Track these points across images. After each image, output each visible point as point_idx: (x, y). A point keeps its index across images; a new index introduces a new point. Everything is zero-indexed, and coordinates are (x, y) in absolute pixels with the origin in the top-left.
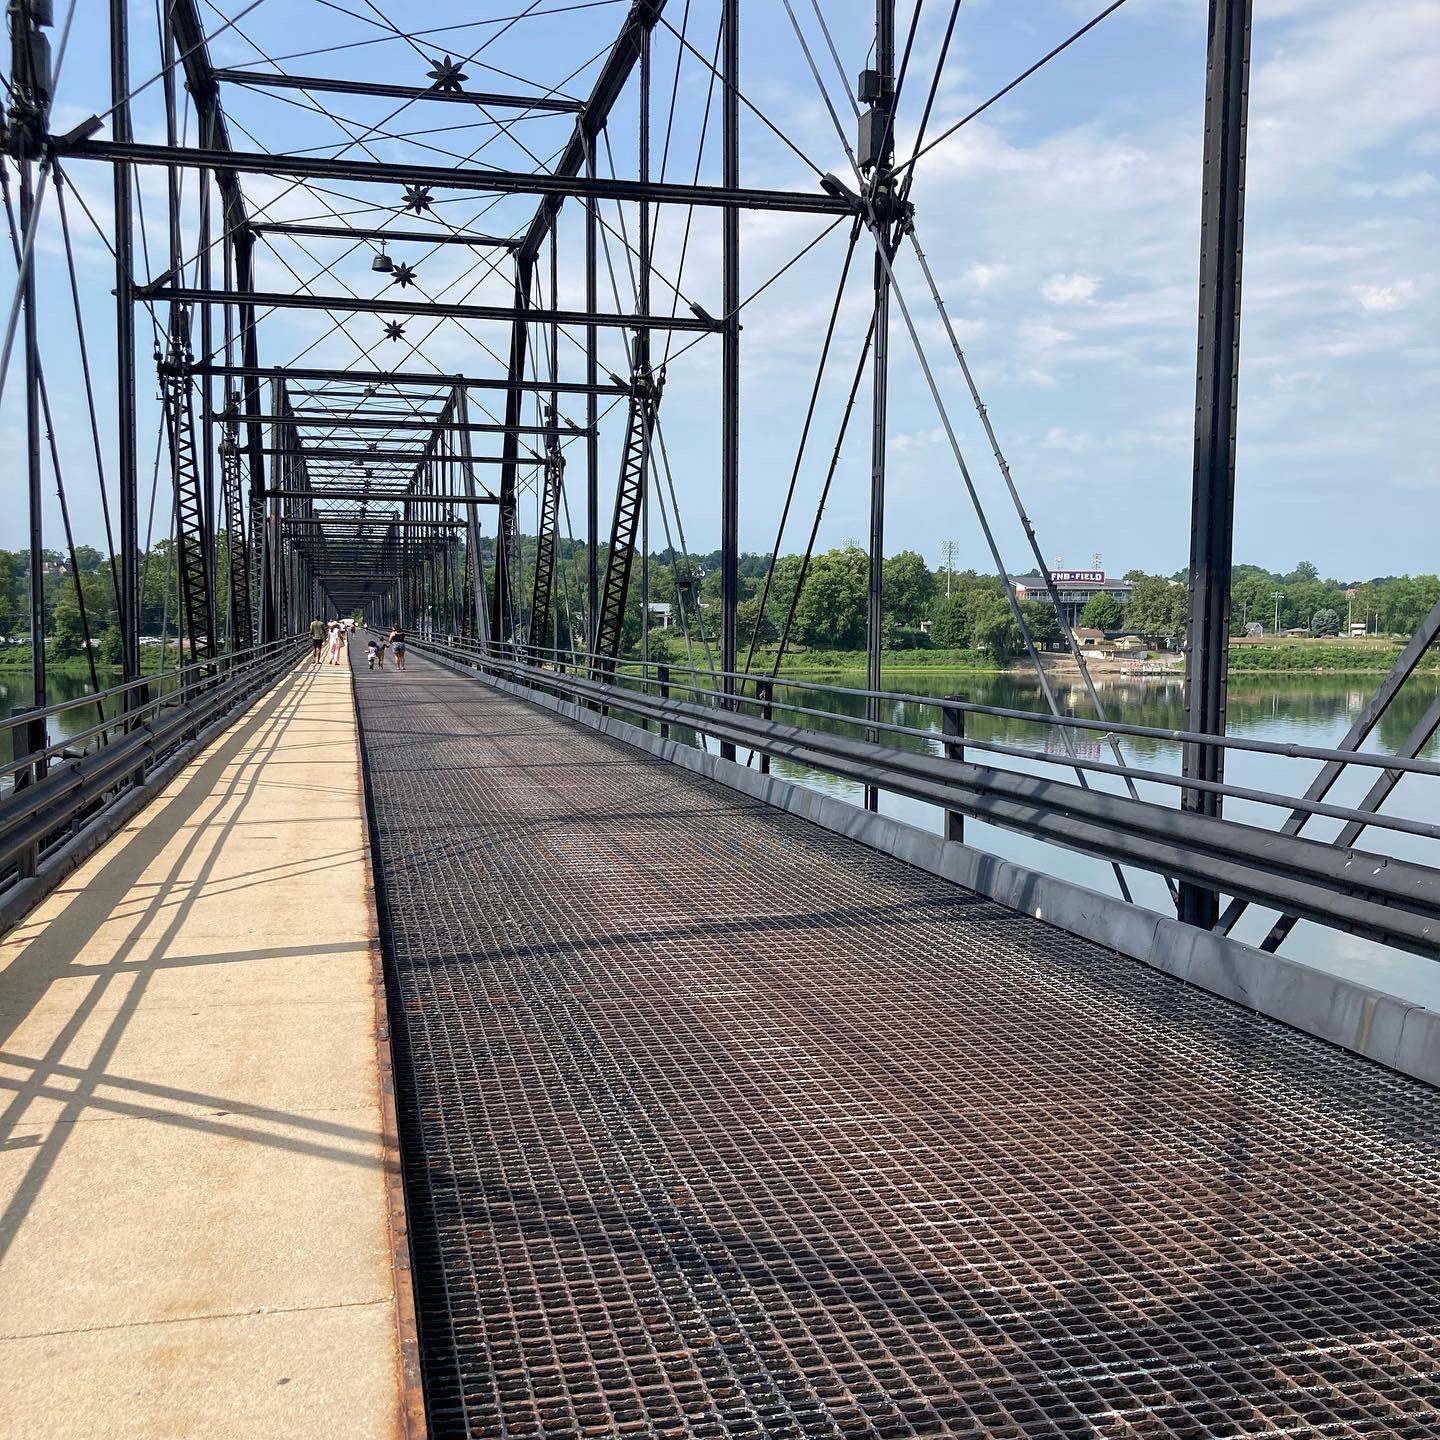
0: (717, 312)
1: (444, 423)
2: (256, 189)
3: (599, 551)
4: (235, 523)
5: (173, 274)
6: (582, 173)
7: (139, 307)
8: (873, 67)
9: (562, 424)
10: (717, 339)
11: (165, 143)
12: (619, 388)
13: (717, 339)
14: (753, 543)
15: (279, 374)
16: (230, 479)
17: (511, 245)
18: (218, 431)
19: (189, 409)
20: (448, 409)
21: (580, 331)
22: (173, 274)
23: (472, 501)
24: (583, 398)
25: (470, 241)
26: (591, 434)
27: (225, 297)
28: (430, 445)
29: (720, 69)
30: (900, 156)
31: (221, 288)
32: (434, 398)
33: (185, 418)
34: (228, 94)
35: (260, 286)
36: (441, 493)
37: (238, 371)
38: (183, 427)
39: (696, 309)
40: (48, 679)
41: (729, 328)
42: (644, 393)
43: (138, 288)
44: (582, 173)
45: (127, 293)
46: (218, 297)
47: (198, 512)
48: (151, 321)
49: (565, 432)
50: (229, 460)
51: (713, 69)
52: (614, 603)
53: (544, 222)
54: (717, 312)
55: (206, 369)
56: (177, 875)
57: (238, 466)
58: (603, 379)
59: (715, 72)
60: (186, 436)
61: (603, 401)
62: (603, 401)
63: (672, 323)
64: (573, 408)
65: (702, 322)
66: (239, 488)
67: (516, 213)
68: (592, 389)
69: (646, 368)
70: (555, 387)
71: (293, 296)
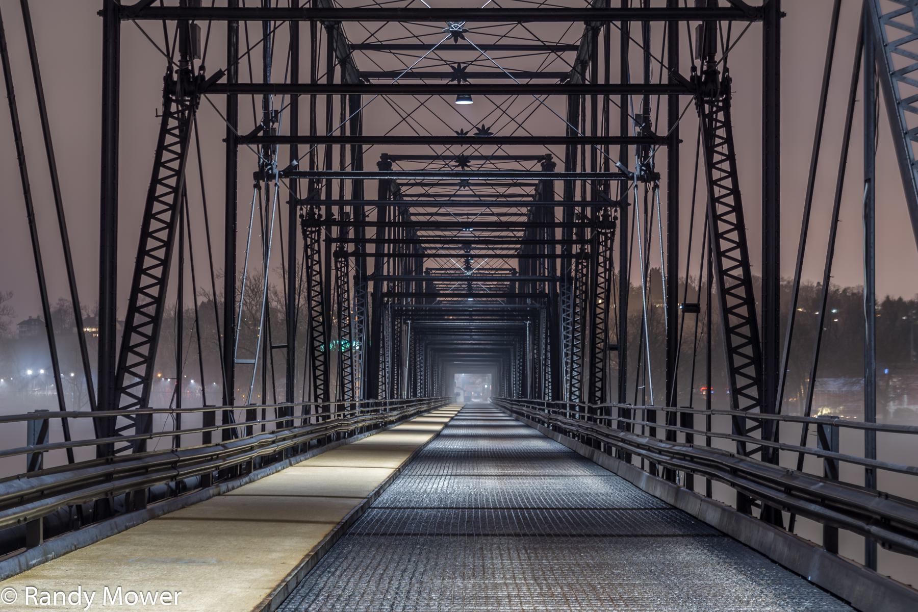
2: (353, 31)
4: (308, 233)
7: (242, 149)
11: (250, 82)
16: (341, 276)
18: (334, 247)
19: (319, 252)
27: (342, 140)
29: (543, 6)
31: (586, 146)
33: (316, 257)
35: (367, 131)
36: (392, 207)
37: (348, 203)
38: (315, 263)
43: (334, 239)
46: (336, 140)
47: (321, 293)
50: (341, 262)
51: (543, 4)
52: (601, 321)
57: (347, 265)
59: (541, 4)
60: (316, 268)
66: (347, 274)
71: (384, 137)
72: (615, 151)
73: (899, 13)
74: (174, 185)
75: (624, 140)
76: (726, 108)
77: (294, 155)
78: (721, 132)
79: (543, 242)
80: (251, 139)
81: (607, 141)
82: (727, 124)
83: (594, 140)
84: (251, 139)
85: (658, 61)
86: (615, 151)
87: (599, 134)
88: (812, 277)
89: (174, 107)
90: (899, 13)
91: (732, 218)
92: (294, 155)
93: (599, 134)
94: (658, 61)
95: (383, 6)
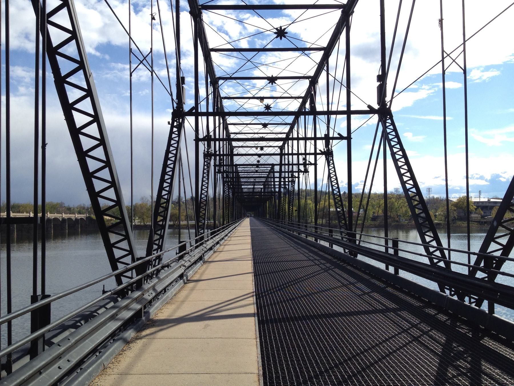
0: (345, 134)
1: (270, 172)
3: (318, 192)
5: (196, 107)
6: (291, 136)
7: (200, 143)
8: (327, 133)
9: (307, 162)
10: (345, 142)
12: (322, 153)
13: (345, 142)
14: (357, 189)
15: (236, 165)
17: (279, 147)
20: (271, 169)
21: (296, 156)
22: (196, 107)
23: (315, 154)
24: (313, 156)
25: (292, 98)
26: (315, 164)
28: (268, 175)
30: (388, 99)
32: (269, 167)
34: (214, 55)
39: (339, 134)
40: (334, 205)
41: (349, 138)
42: (328, 154)
44: (291, 136)
45: (197, 140)
48: (202, 146)
49: (308, 164)
53: (284, 144)
54: (345, 134)
55: (215, 155)
56: (303, 101)
58: (318, 151)
61: (318, 156)
62: (318, 156)
63: (334, 138)
64: (311, 159)
65: (341, 137)
67: (290, 119)
68: (315, 154)
69: (329, 148)
70: (306, 154)
72: (295, 157)
73: (438, 262)
74: (175, 153)
75: (215, 140)
76: (333, 158)
77: (209, 146)
78: (331, 162)
79: (271, 178)
80: (203, 139)
81: (293, 154)
82: (333, 160)
83: (288, 154)
84: (203, 139)
85: (132, 53)
86: (295, 157)
87: (221, 138)
88: (304, 188)
89: (175, 124)
90: (438, 262)
91: (333, 169)
92: (209, 146)
93: (221, 138)
94: (132, 53)
95: (231, 96)
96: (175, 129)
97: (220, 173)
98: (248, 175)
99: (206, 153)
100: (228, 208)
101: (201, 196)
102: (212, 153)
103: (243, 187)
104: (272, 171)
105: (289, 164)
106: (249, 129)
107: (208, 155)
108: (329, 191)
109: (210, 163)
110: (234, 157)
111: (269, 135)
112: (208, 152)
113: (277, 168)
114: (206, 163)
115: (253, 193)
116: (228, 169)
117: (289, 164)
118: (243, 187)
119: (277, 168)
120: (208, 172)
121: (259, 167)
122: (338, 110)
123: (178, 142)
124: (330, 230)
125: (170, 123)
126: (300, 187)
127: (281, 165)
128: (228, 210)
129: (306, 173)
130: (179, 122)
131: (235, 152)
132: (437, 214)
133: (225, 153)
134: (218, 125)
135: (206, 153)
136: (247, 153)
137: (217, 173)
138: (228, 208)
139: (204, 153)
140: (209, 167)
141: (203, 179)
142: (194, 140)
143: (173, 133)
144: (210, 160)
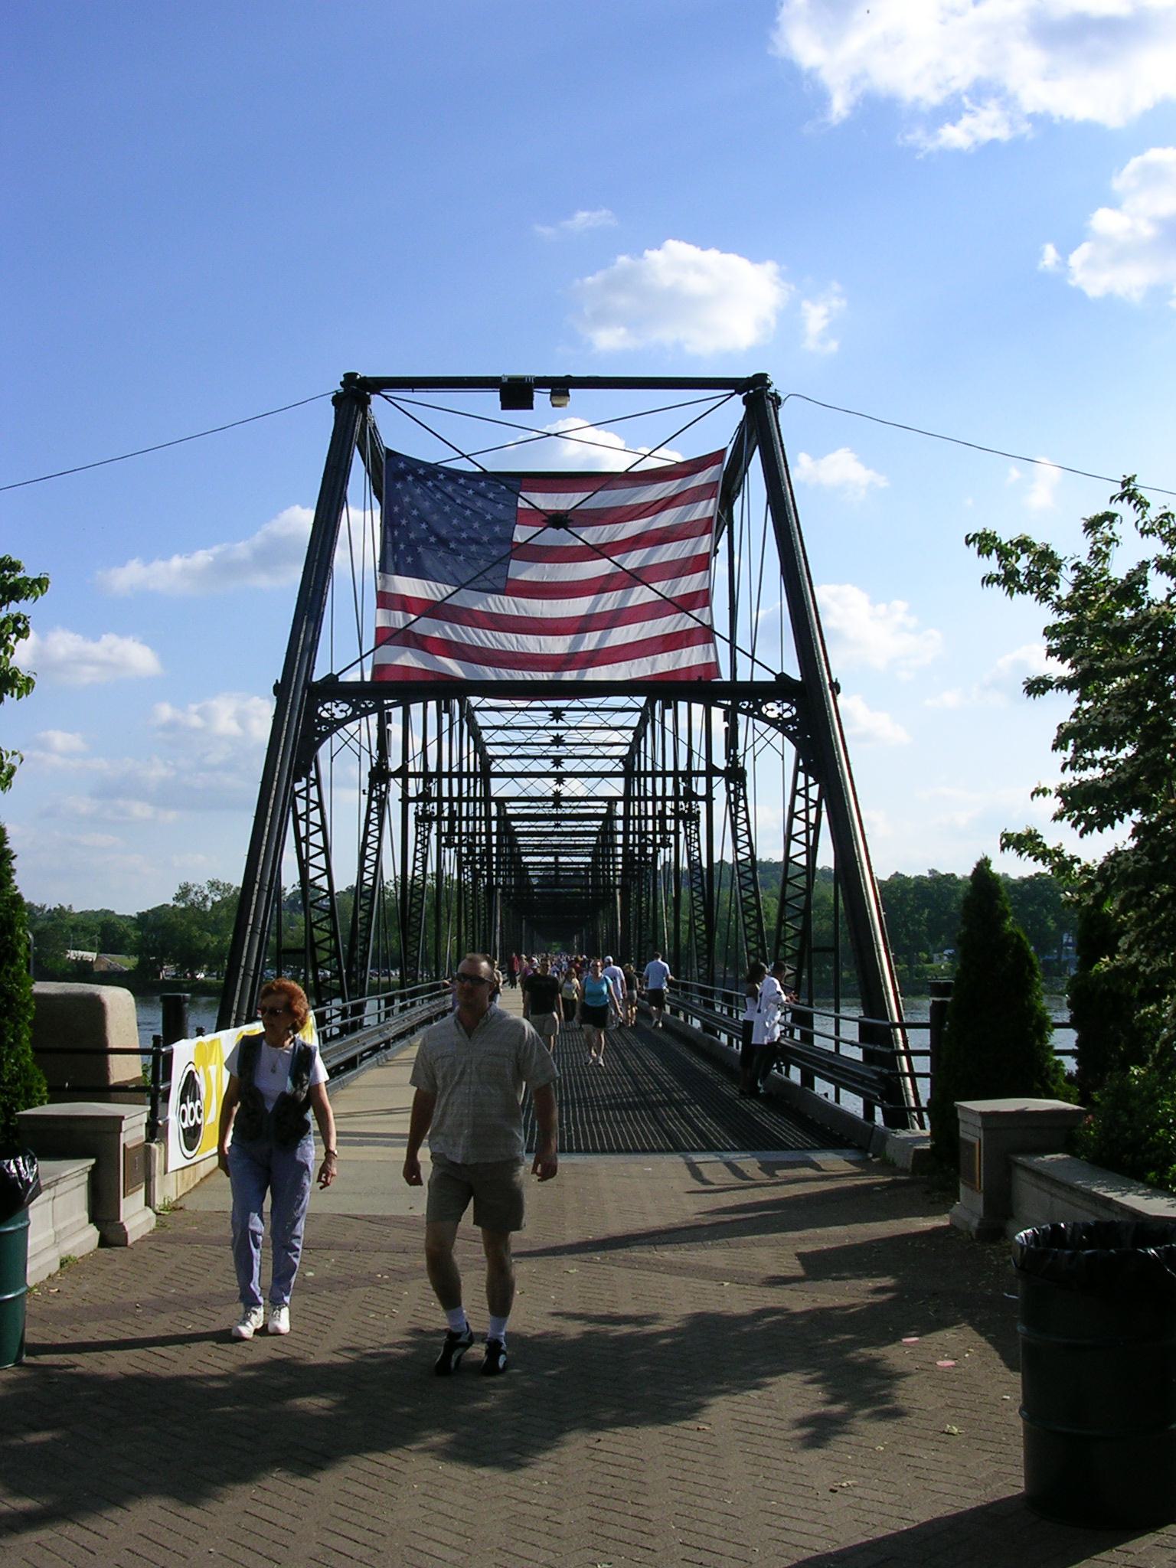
5: (405, 766)
22: (405, 766)
32: (601, 807)
96: (373, 816)
97: (450, 847)
98: (533, 826)
99: (420, 813)
100: (473, 926)
101: (411, 900)
102: (433, 813)
103: (526, 859)
104: (609, 818)
105: (654, 799)
106: (528, 719)
107: (423, 819)
108: (810, 867)
109: (428, 837)
110: (493, 781)
111: (595, 706)
112: (424, 811)
113: (620, 809)
114: (419, 836)
115: (555, 875)
116: (475, 809)
117: (654, 799)
118: (526, 859)
119: (620, 809)
120: (425, 856)
121: (561, 807)
122: (755, 679)
123: (379, 839)
124: (712, 985)
125: (367, 792)
126: (716, 859)
127: (627, 798)
128: (473, 933)
129: (665, 848)
130: (380, 790)
131: (494, 768)
132: (12, 970)
133: (472, 770)
134: (447, 727)
135: (420, 813)
136: (526, 770)
137: (445, 845)
138: (473, 926)
139: (416, 814)
140: (427, 846)
141: (415, 855)
142: (400, 800)
143: (372, 810)
144: (429, 830)
